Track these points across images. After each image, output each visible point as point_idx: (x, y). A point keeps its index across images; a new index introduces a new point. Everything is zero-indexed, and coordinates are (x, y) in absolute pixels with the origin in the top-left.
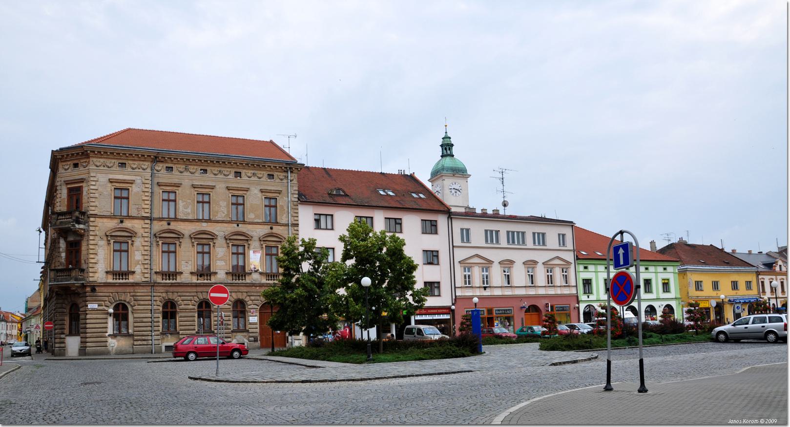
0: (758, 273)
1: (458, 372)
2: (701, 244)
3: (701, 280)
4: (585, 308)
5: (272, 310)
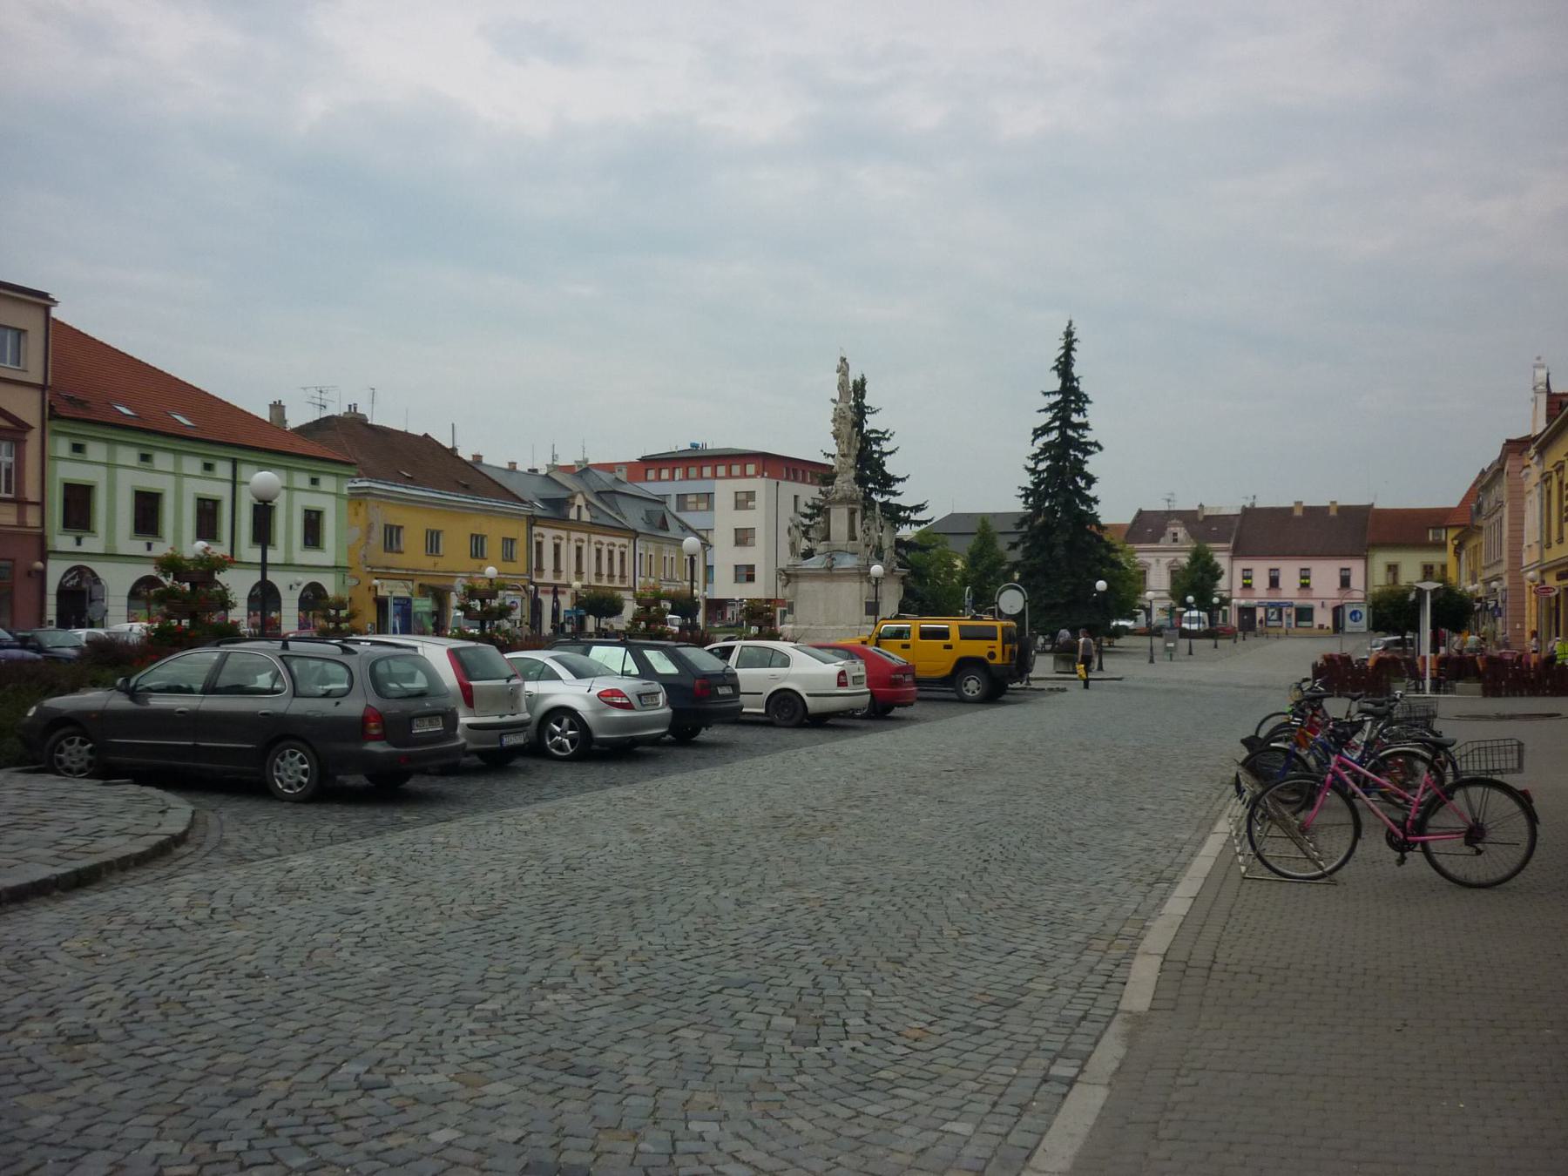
2: (402, 429)
3: (398, 524)
4: (65, 575)
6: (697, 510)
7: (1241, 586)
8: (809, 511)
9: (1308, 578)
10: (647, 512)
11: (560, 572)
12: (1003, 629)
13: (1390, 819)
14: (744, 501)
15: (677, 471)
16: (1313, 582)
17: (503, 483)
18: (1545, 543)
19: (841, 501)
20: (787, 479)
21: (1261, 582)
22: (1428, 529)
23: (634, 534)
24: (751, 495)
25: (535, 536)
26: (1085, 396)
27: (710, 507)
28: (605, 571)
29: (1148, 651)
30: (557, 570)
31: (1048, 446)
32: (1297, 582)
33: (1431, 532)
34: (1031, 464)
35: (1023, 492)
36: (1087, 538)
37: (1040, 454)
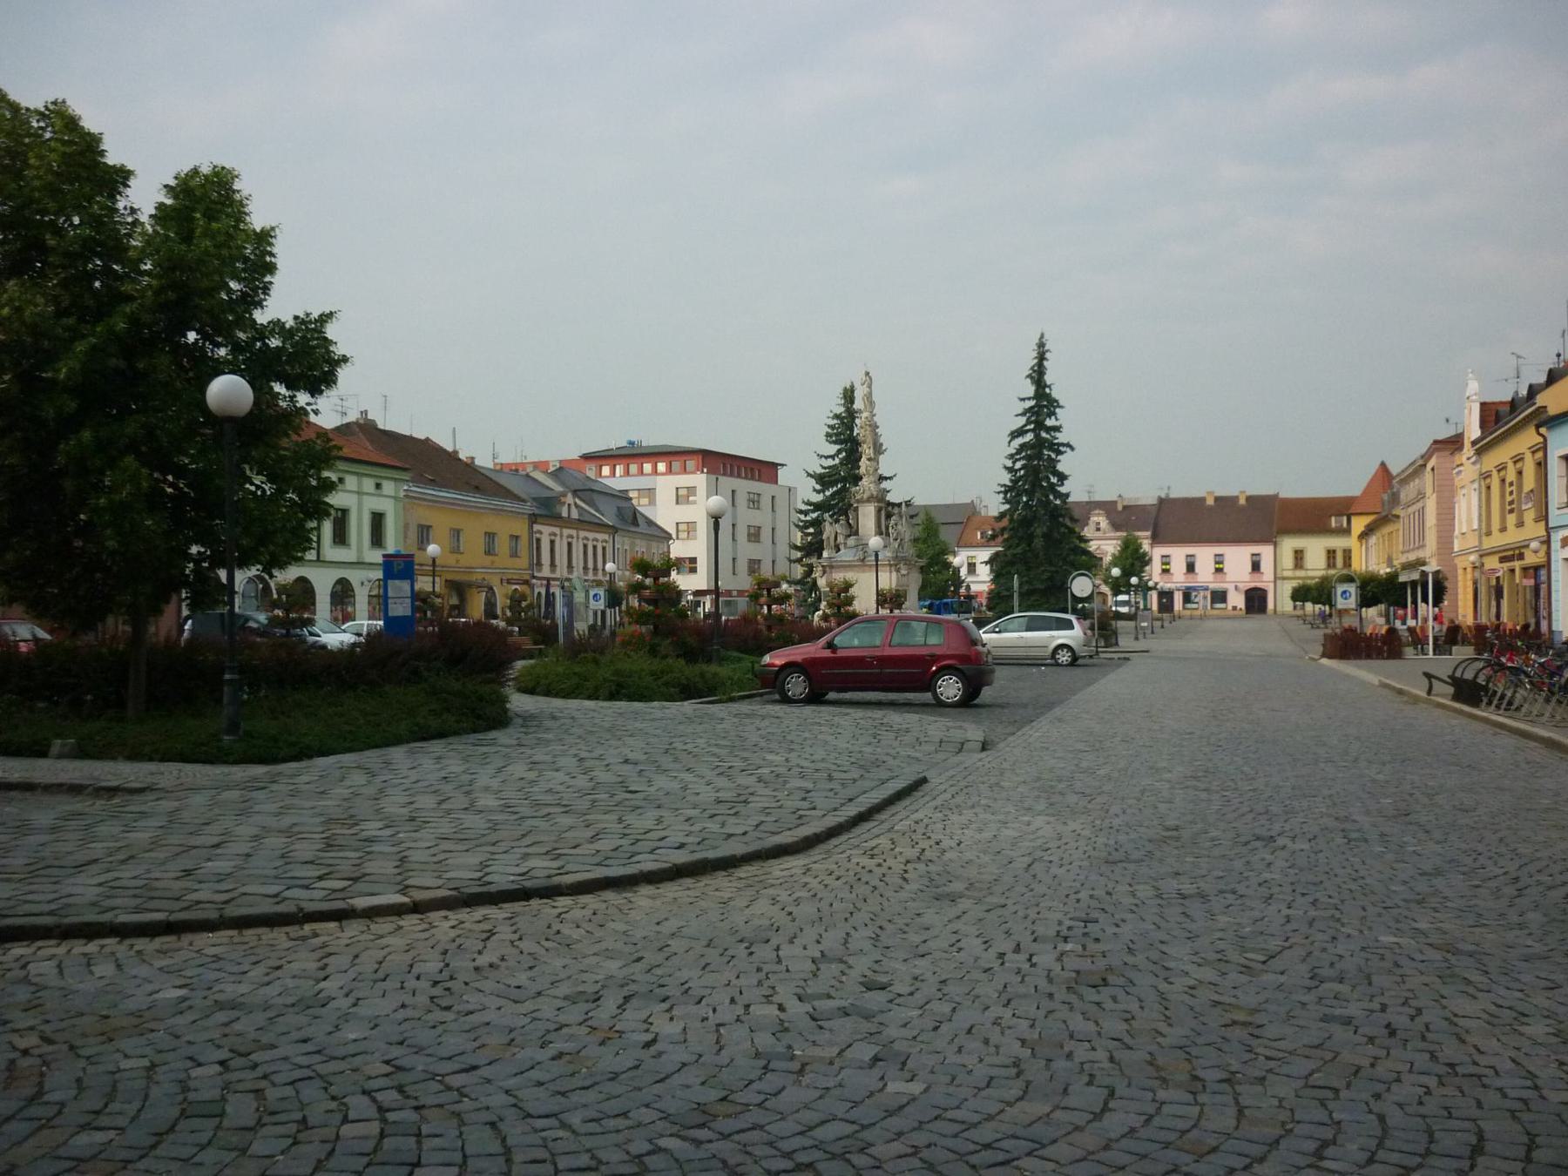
1: (568, 1153)
2: (408, 434)
3: (428, 524)
7: (1160, 571)
8: (804, 507)
9: (1222, 563)
10: (618, 508)
11: (555, 566)
12: (368, 625)
13: (450, 889)
15: (618, 467)
16: (1227, 567)
17: (494, 478)
18: (1484, 531)
19: (869, 500)
20: (724, 474)
21: (1178, 567)
22: (1330, 516)
23: (613, 530)
24: (692, 490)
26: (1057, 401)
28: (590, 565)
29: (1134, 631)
30: (553, 565)
31: (1023, 447)
32: (1211, 567)
33: (1333, 519)
34: (1009, 463)
35: (1003, 489)
36: (1062, 530)
37: (1017, 454)
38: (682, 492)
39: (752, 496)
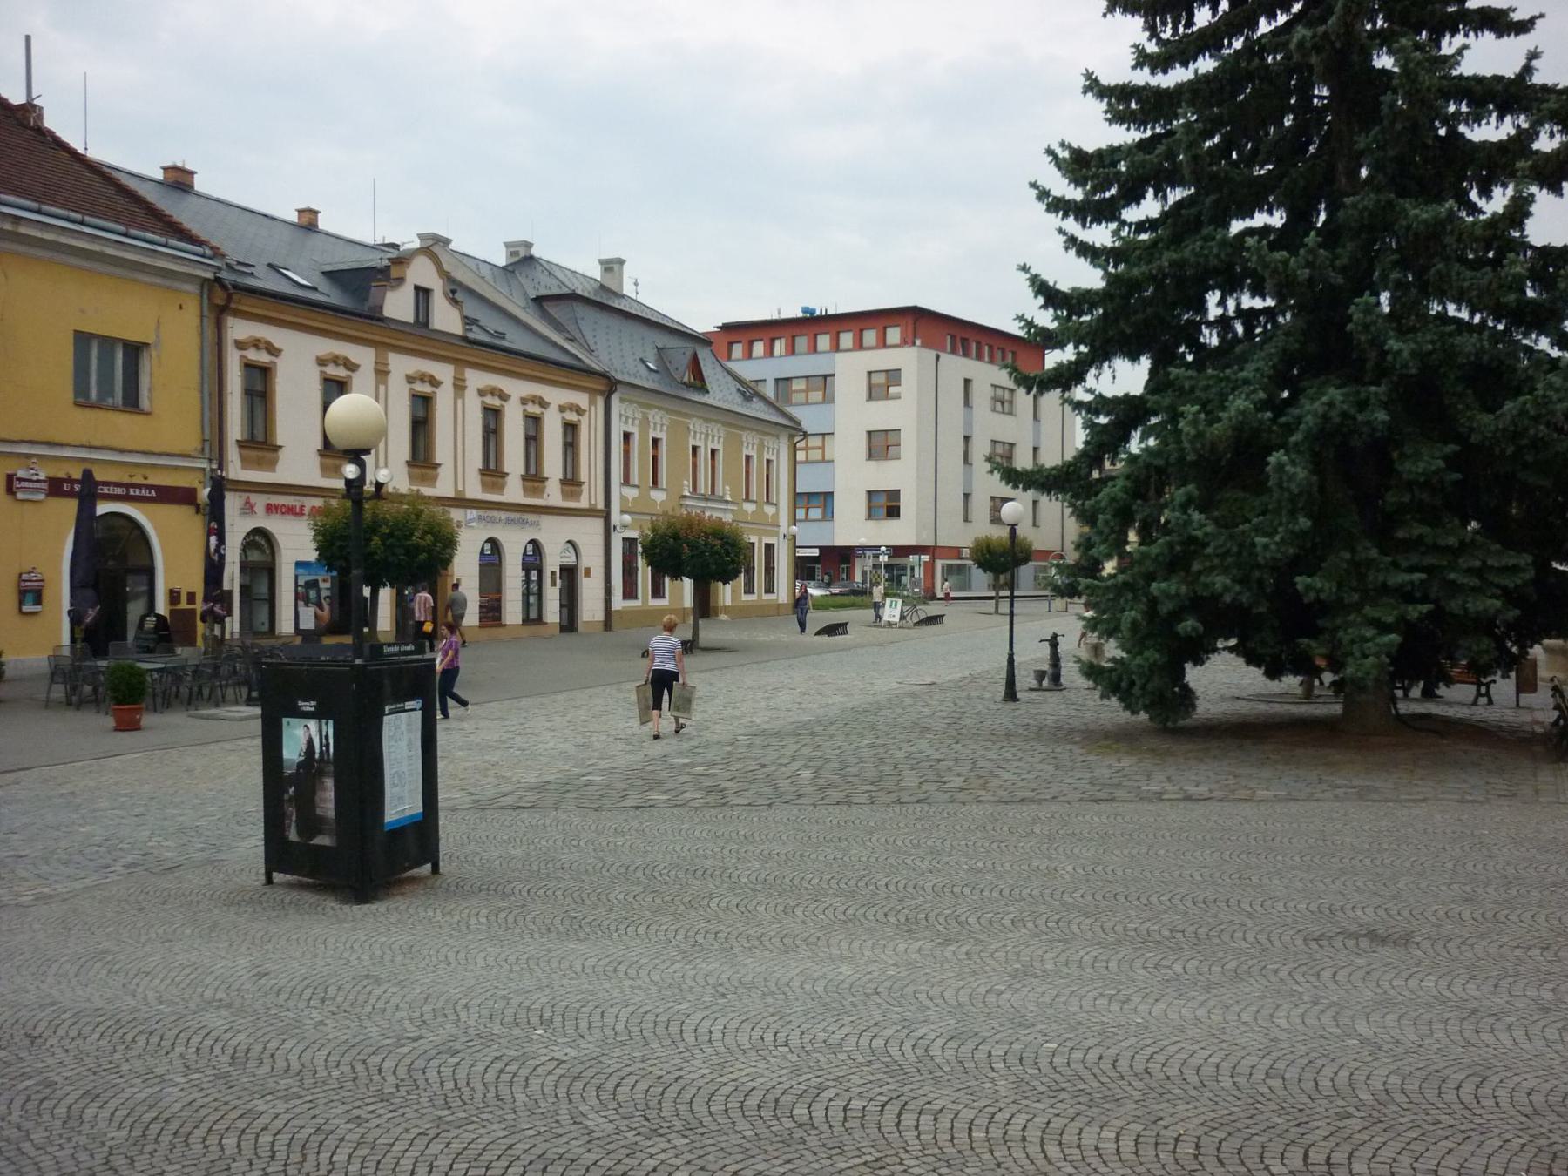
0: (220, 299)
5: (1012, 593)
6: (807, 403)
14: (882, 386)
15: (777, 344)
20: (954, 351)
24: (893, 376)
25: (240, 345)
27: (828, 399)
38: (880, 379)
39: (999, 392)
